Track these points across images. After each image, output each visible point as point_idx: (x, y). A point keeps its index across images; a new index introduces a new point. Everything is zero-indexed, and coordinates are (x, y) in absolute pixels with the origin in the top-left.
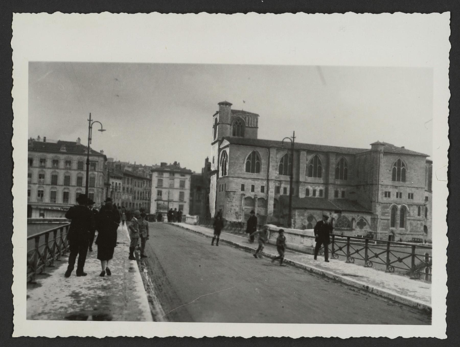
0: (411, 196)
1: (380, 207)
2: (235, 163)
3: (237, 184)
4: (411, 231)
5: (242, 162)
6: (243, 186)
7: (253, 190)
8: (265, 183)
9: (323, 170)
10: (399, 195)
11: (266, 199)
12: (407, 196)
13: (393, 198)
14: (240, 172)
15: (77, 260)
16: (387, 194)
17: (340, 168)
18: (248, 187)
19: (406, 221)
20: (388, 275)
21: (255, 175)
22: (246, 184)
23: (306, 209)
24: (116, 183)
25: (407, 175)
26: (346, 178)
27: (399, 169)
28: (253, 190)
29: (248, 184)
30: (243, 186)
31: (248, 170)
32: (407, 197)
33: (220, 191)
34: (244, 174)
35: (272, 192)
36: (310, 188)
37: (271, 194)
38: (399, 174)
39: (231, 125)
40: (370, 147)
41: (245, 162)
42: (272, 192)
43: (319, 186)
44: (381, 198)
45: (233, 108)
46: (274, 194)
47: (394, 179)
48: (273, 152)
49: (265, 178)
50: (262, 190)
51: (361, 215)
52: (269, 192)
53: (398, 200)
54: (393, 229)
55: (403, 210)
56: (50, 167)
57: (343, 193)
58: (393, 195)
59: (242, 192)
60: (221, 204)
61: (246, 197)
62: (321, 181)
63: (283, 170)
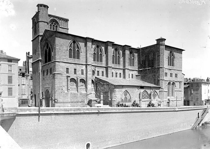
0: (176, 75)
1: (165, 83)
2: (60, 49)
3: (62, 67)
7: (75, 73)
8: (84, 67)
9: (122, 59)
15: (48, 54)
16: (166, 74)
18: (71, 70)
20: (99, 104)
21: (76, 61)
22: (69, 68)
25: (175, 62)
27: (171, 57)
28: (75, 73)
35: (90, 74)
37: (89, 76)
38: (171, 62)
40: (155, 43)
41: (68, 50)
42: (90, 74)
45: (50, 12)
48: (89, 44)
50: (82, 74)
52: (88, 74)
54: (169, 97)
55: (173, 84)
59: (68, 75)
61: (71, 78)
62: (122, 67)
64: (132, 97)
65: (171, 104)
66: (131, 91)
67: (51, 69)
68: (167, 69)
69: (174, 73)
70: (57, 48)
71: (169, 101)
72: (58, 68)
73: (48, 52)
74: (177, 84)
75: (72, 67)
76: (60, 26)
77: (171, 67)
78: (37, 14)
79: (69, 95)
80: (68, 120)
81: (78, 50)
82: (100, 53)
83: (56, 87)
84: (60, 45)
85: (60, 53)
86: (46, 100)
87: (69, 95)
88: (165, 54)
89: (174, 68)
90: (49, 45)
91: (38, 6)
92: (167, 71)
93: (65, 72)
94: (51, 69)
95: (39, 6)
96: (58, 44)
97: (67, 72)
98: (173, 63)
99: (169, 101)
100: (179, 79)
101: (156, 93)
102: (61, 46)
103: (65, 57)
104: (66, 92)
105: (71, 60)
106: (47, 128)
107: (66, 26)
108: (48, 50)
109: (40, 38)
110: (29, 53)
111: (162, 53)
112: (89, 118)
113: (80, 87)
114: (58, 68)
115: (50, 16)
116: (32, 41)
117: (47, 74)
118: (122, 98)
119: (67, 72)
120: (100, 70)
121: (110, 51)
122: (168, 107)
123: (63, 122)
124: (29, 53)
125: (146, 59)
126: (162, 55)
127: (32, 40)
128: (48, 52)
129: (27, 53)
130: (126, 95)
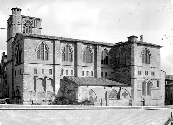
0: (153, 74)
4: (153, 98)
5: (34, 51)
6: (36, 70)
7: (43, 73)
8: (52, 68)
10: (146, 73)
11: (53, 79)
12: (144, 73)
13: (143, 74)
14: (33, 59)
16: (140, 73)
17: (103, 56)
18: (39, 71)
19: (151, 90)
21: (45, 62)
23: (87, 85)
24: (88, 72)
26: (107, 64)
28: (43, 73)
29: (40, 67)
30: (36, 70)
31: (39, 57)
32: (151, 74)
33: (16, 75)
34: (36, 60)
36: (65, 69)
38: (147, 59)
39: (21, 25)
40: (127, 40)
42: (104, 74)
43: (90, 69)
44: (137, 75)
46: (59, 75)
47: (143, 62)
49: (52, 63)
51: (125, 88)
53: (146, 76)
55: (150, 82)
56: (27, 40)
57: (106, 73)
58: (143, 73)
59: (35, 75)
60: (18, 85)
62: (93, 65)
63: (65, 57)
64: (98, 96)
65: (146, 103)
66: (97, 90)
67: (21, 69)
68: (141, 67)
69: (150, 71)
70: (25, 50)
71: (144, 101)
72: (26, 69)
73: (19, 53)
74: (154, 83)
75: (40, 67)
76: (33, 27)
77: (145, 65)
78: (11, 17)
79: (37, 95)
80: (25, 115)
81: (46, 51)
82: (70, 53)
83: (24, 87)
84: (28, 48)
85: (28, 55)
86: (17, 99)
87: (37, 95)
88: (138, 52)
89: (151, 65)
90: (20, 47)
91: (12, 9)
92: (141, 69)
93: (33, 72)
94: (21, 69)
95: (14, 9)
96: (26, 47)
97: (36, 72)
98: (149, 60)
99: (144, 101)
100: (157, 76)
101: (127, 92)
102: (29, 49)
103: (33, 58)
104: (34, 91)
105: (39, 61)
106: (7, 120)
107: (39, 26)
108: (19, 51)
109: (13, 39)
110: (4, 52)
111: (133, 52)
112: (43, 114)
113: (48, 86)
114: (26, 69)
115: (23, 17)
116: (7, 41)
117: (18, 75)
118: (87, 97)
119: (36, 72)
120: (69, 69)
121: (80, 50)
122: (101, 106)
123: (20, 116)
124: (4, 52)
125: (120, 57)
126: (133, 53)
127: (7, 40)
128: (19, 53)
129: (3, 53)
130: (90, 93)
